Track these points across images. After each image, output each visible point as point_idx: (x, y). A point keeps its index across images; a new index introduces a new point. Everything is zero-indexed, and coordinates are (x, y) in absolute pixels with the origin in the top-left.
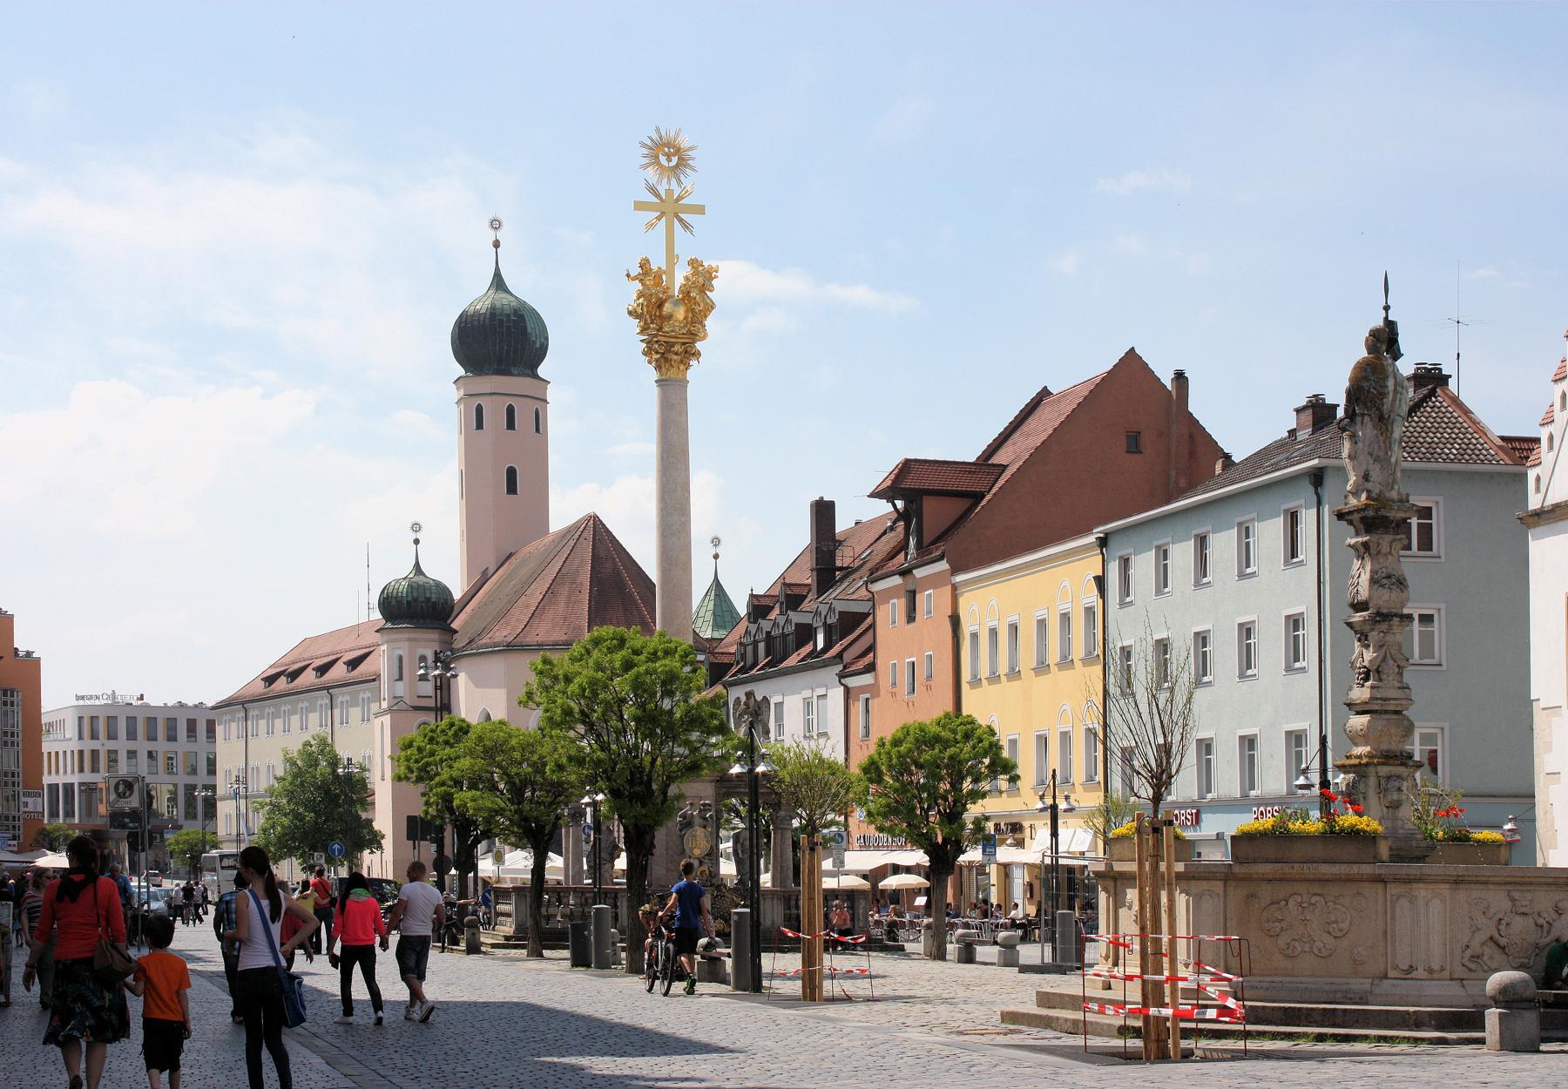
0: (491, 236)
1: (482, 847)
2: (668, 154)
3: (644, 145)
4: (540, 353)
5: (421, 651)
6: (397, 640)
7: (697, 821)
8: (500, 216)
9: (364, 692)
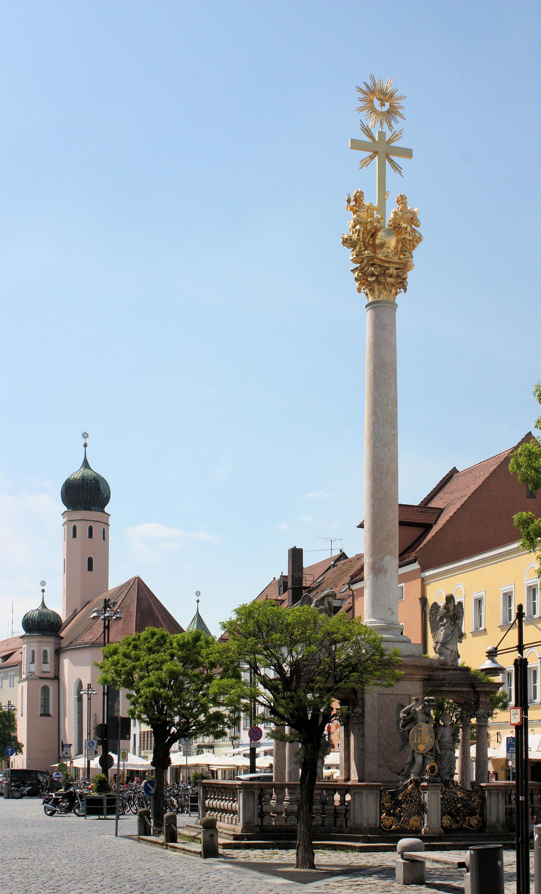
0: (83, 441)
1: (175, 746)
2: (381, 100)
3: (360, 90)
4: (106, 500)
5: (44, 648)
6: (31, 642)
7: (421, 717)
8: (87, 432)
9: (11, 672)
